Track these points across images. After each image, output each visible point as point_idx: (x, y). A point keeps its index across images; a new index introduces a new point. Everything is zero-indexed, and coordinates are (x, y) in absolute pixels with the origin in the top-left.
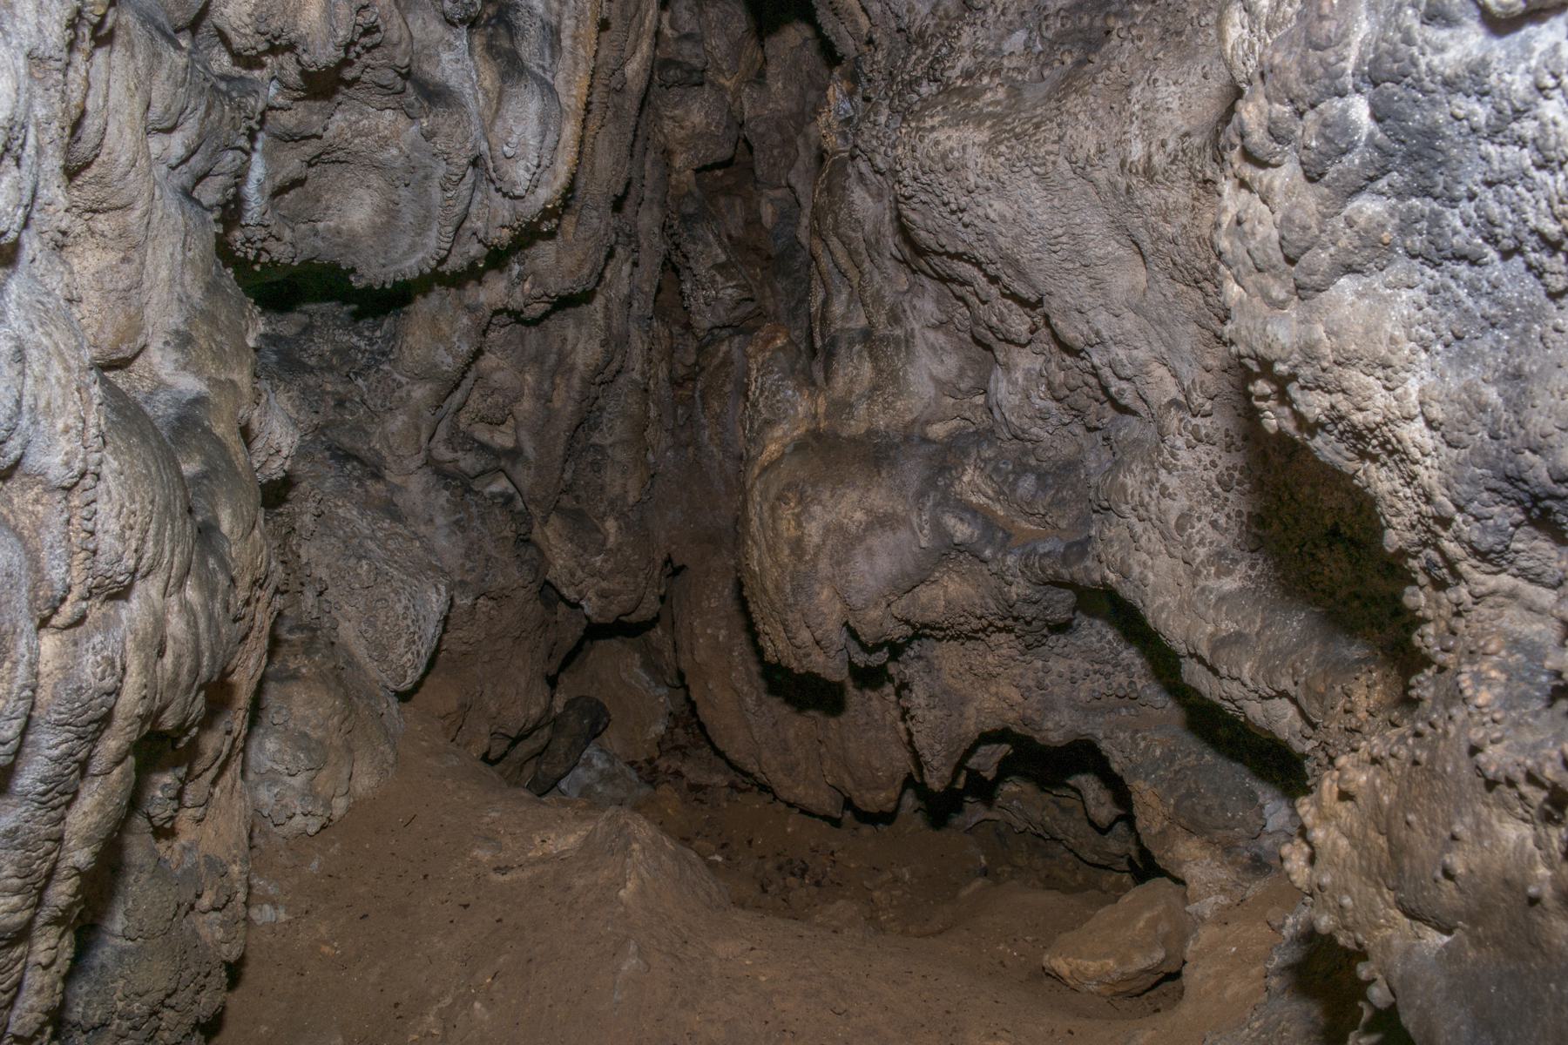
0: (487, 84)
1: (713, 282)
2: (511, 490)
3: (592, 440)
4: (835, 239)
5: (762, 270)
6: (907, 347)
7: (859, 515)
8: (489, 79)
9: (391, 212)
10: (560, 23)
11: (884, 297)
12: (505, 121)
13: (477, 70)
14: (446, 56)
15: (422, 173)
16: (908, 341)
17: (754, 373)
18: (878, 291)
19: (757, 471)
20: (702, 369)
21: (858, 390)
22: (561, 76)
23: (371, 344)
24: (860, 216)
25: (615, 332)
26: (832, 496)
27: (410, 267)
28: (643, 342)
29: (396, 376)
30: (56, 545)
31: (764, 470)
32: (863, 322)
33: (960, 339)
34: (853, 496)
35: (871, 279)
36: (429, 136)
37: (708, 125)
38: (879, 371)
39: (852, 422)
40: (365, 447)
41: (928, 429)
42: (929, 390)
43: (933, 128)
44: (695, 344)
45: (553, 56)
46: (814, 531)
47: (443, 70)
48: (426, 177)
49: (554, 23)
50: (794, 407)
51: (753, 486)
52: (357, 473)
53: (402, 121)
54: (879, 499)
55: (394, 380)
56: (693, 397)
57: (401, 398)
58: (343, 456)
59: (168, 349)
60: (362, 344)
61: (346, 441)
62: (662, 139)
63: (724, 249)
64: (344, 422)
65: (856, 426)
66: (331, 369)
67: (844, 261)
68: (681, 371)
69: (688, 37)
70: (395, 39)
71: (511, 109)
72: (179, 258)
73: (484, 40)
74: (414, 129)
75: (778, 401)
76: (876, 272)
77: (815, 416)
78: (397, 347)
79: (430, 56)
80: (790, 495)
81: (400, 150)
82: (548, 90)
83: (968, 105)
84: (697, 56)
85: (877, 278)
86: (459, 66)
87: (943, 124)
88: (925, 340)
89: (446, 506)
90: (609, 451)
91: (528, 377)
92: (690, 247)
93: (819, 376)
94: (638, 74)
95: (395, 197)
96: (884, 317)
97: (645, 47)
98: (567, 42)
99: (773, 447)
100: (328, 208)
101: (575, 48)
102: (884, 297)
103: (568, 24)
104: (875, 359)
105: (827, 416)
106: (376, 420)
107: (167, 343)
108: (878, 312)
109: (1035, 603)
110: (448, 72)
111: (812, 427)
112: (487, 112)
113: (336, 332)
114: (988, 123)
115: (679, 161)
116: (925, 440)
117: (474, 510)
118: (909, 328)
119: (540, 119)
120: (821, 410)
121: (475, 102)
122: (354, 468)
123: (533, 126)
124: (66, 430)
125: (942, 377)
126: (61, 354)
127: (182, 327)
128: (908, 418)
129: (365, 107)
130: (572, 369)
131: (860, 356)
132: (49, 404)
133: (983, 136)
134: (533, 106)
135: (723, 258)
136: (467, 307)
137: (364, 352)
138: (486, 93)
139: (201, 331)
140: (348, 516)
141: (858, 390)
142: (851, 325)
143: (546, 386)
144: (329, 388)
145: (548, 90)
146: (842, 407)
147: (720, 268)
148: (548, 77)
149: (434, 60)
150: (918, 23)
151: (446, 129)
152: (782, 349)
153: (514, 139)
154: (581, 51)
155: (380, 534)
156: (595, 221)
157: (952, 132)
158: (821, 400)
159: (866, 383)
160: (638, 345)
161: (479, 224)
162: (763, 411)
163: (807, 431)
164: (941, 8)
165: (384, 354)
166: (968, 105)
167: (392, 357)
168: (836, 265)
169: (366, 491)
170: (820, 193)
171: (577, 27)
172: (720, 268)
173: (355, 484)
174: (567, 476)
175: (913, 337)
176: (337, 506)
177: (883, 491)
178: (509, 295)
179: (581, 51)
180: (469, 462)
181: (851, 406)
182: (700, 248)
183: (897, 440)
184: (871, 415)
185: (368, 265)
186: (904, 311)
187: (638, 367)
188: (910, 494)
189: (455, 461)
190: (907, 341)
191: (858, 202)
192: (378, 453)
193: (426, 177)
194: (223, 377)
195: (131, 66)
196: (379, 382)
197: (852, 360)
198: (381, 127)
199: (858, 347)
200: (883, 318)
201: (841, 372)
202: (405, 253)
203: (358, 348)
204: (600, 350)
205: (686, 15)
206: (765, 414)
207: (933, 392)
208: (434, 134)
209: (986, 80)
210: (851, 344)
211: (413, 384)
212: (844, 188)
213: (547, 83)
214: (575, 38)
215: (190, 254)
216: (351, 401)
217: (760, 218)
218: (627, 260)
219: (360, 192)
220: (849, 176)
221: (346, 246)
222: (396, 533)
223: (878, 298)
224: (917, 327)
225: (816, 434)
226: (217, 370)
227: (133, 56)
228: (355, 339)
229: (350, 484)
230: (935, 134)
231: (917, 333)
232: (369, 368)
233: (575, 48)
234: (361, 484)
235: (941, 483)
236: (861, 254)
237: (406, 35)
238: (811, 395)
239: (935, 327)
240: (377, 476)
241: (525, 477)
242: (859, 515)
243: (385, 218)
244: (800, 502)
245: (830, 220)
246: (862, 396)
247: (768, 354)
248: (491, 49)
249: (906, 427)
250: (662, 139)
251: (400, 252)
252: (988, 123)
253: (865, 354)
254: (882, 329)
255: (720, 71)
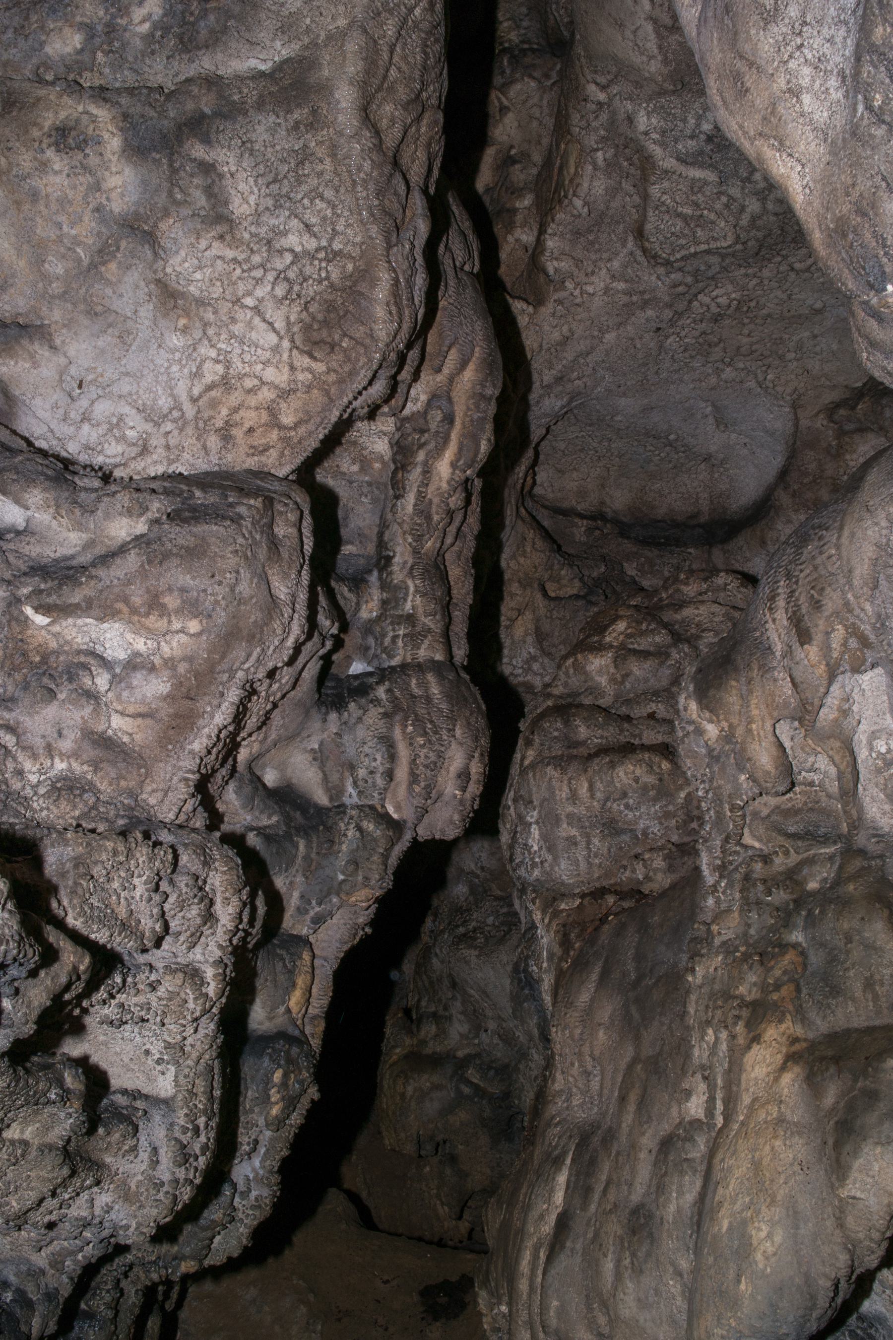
7: (428, 1084)
31: (391, 1066)
34: (426, 1076)
42: (457, 1037)
46: (410, 1090)
54: (436, 1079)
65: (428, 1051)
93: (415, 1030)
104: (437, 1024)
109: (127, 374)
116: (455, 1057)
133: (477, 953)
146: (424, 1043)
206: (393, 1043)
242: (428, 1084)
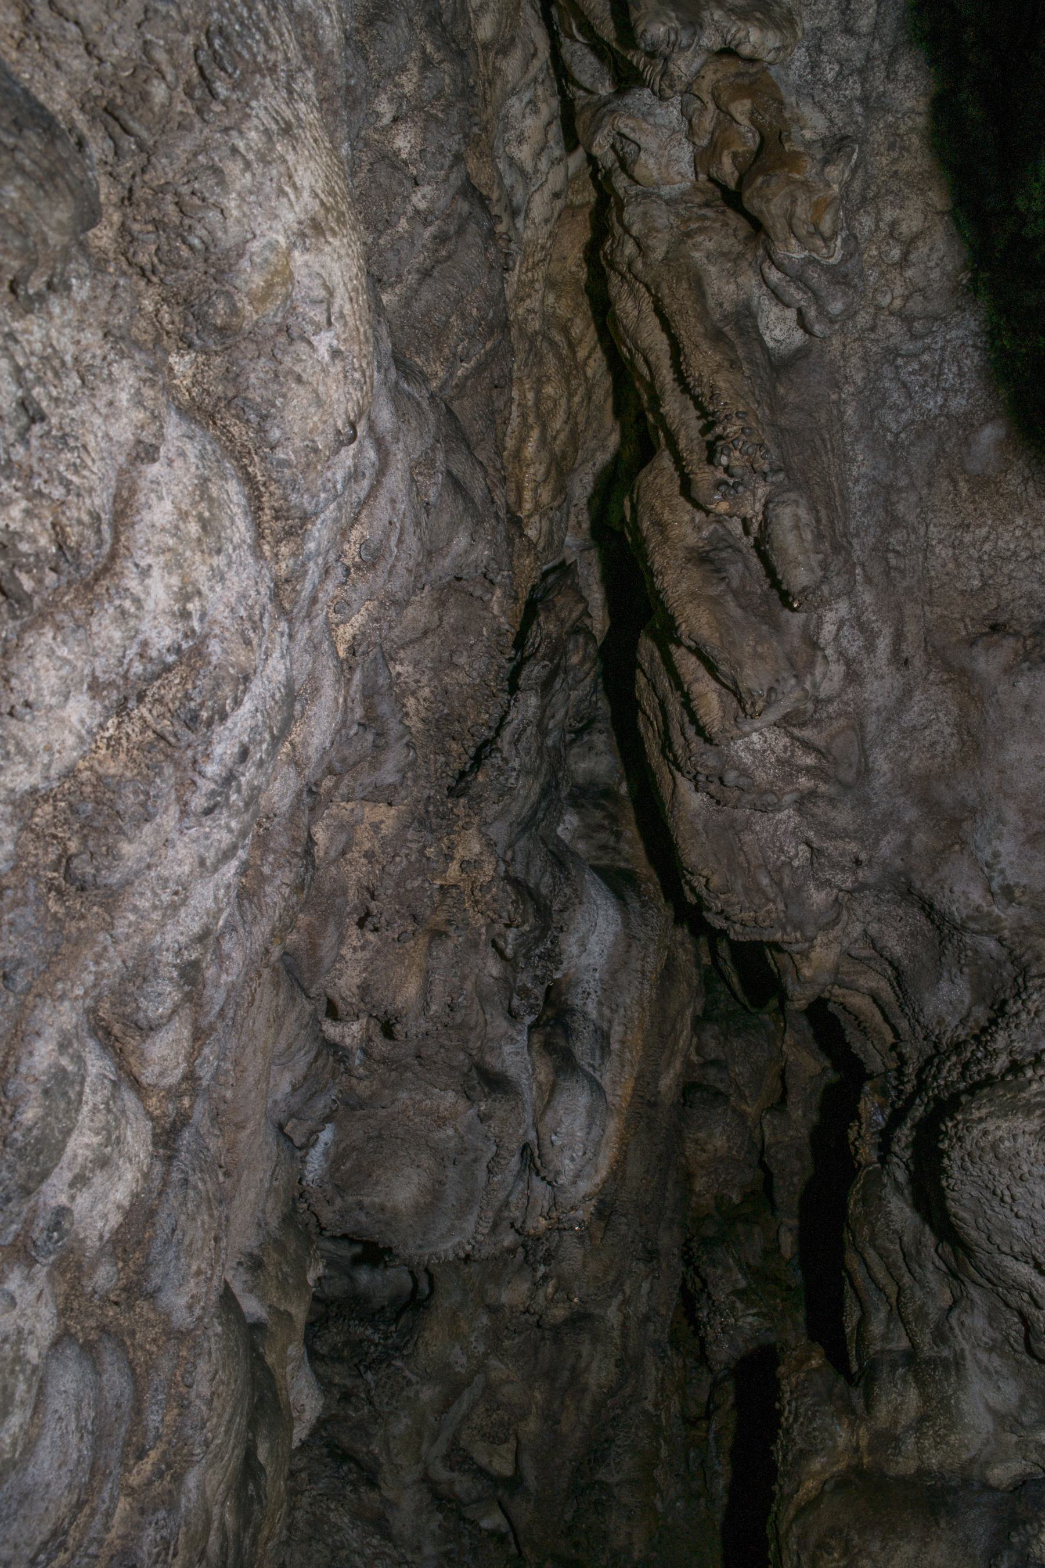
0: (542, 1077)
1: (733, 1308)
2: (505, 1527)
3: (599, 1476)
4: (872, 1252)
5: (783, 1300)
6: (958, 1370)
8: (544, 1075)
9: (435, 1192)
10: (610, 1028)
11: (927, 1314)
12: (556, 1112)
13: (533, 1065)
14: (507, 1049)
15: (472, 1156)
16: (957, 1364)
17: (787, 1395)
18: (921, 1307)
19: (792, 1512)
20: (718, 1407)
21: (904, 1420)
22: (608, 1076)
23: (386, 1338)
24: (898, 1226)
25: (630, 1352)
26: (883, 1549)
27: (446, 1251)
28: (658, 1369)
29: (407, 1373)
30: (161, 1389)
31: (801, 1510)
32: (905, 1343)
33: (1017, 1361)
35: (913, 1296)
36: (483, 1118)
37: (730, 1148)
38: (926, 1399)
39: (900, 1459)
40: (364, 1450)
41: (989, 1473)
42: (986, 1423)
43: (981, 1120)
44: (710, 1380)
45: (602, 1058)
47: (503, 1061)
48: (475, 1160)
49: (605, 1028)
50: (833, 1438)
51: (789, 1529)
52: (353, 1476)
53: (462, 1104)
55: (404, 1377)
56: (706, 1439)
57: (409, 1398)
58: (341, 1455)
59: (241, 1269)
60: (376, 1337)
61: (345, 1439)
62: (684, 1161)
63: (745, 1276)
64: (347, 1418)
65: (905, 1465)
66: (340, 1359)
67: (881, 1275)
68: (695, 1411)
69: (714, 1063)
70: (472, 1023)
71: (562, 1100)
72: (267, 1185)
73: (542, 1038)
74: (472, 1112)
75: (814, 1429)
76: (917, 1287)
77: (857, 1449)
78: (412, 1342)
79: (493, 1049)
80: (833, 1543)
81: (456, 1130)
82: (597, 1088)
83: (1015, 1097)
84: (722, 1080)
85: (919, 1294)
86: (518, 1058)
87: (990, 1115)
88: (978, 1362)
89: (438, 1532)
90: (616, 1491)
91: (538, 1395)
92: (710, 1270)
93: (859, 1403)
94: (670, 1088)
95: (442, 1177)
96: (929, 1336)
97: (678, 1064)
98: (615, 1046)
99: (810, 1484)
100: (377, 1183)
101: (622, 1052)
102: (927, 1314)
103: (617, 1030)
104: (921, 1384)
105: (872, 1450)
106: (380, 1420)
107: (240, 1263)
108: (921, 1330)
110: (508, 1063)
111: (855, 1462)
112: (538, 1103)
113: (352, 1323)
114: (1038, 1112)
115: (700, 1184)
116: (987, 1487)
117: (466, 1541)
118: (957, 1348)
119: (588, 1112)
120: (863, 1443)
121: (530, 1095)
122: (350, 1470)
123: (582, 1120)
124: (199, 1273)
125: (999, 1407)
126: (209, 1201)
127: (256, 1251)
128: (965, 1456)
129: (430, 1088)
130: (584, 1390)
131: (905, 1382)
132: (191, 1244)
134: (583, 1100)
135: (743, 1284)
136: (488, 1306)
137: (377, 1345)
138: (540, 1086)
139: (272, 1258)
140: (339, 1522)
141: (904, 1420)
142: (893, 1346)
143: (556, 1405)
144: (337, 1380)
145: (597, 1088)
147: (740, 1293)
148: (597, 1075)
149: (497, 1052)
150: (948, 1034)
151: (500, 1113)
152: (817, 1370)
153: (563, 1129)
154: (628, 1055)
155: (368, 1551)
156: (624, 1227)
157: (1000, 1122)
158: (862, 1431)
159: (913, 1414)
160: (652, 1373)
161: (518, 1214)
162: (798, 1440)
163: (848, 1466)
164: (971, 1019)
165: (397, 1348)
166: (1015, 1097)
167: (405, 1352)
168: (874, 1281)
169: (360, 1499)
170: (855, 1204)
171: (625, 1033)
172: (740, 1293)
173: (349, 1488)
174: (568, 1517)
175: (963, 1358)
176: (329, 1509)
177: (943, 1547)
178: (532, 1297)
179: (628, 1055)
180: (463, 1485)
181: (897, 1439)
182: (719, 1272)
183: (953, 1483)
184: (921, 1451)
185: (405, 1245)
186: (951, 1328)
187: (651, 1395)
188: (978, 1553)
189: (452, 1483)
190: (957, 1364)
191: (895, 1212)
192: (375, 1459)
193: (475, 1160)
194: (282, 1308)
195: (274, 1004)
196: (389, 1378)
197: (895, 1386)
198: (442, 1108)
199: (901, 1371)
200: (928, 1338)
201: (884, 1399)
202: (443, 1236)
203: (371, 1342)
204: (614, 1370)
205: (712, 1043)
206: (800, 1444)
207: (991, 1427)
208: (491, 1118)
209: (1029, 1073)
210: (894, 1368)
211: (423, 1385)
212: (880, 1198)
213: (595, 1080)
214: (622, 1042)
215: (276, 1183)
216: (358, 1396)
217: (779, 1247)
218: (647, 1277)
219: (409, 1171)
220: (885, 1186)
221: (387, 1224)
222: (384, 1553)
223: (921, 1315)
224: (967, 1347)
225: (857, 1470)
226: (279, 1299)
227: (277, 995)
228: (369, 1332)
229: (344, 1487)
230: (983, 1125)
231: (967, 1353)
232: (381, 1362)
233: (622, 1052)
234: (355, 1490)
235: (1015, 1540)
236: (900, 1268)
237: (481, 1021)
238: (851, 1424)
239: (991, 1350)
240: (372, 1483)
241: (524, 1511)
243: (429, 1199)
244: (845, 1553)
245: (866, 1231)
246: (908, 1428)
247: (802, 1375)
248: (548, 1047)
249: (962, 1468)
250: (684, 1161)
251: (438, 1234)
252: (1038, 1112)
253: (910, 1378)
254: (927, 1350)
255: (742, 1097)
